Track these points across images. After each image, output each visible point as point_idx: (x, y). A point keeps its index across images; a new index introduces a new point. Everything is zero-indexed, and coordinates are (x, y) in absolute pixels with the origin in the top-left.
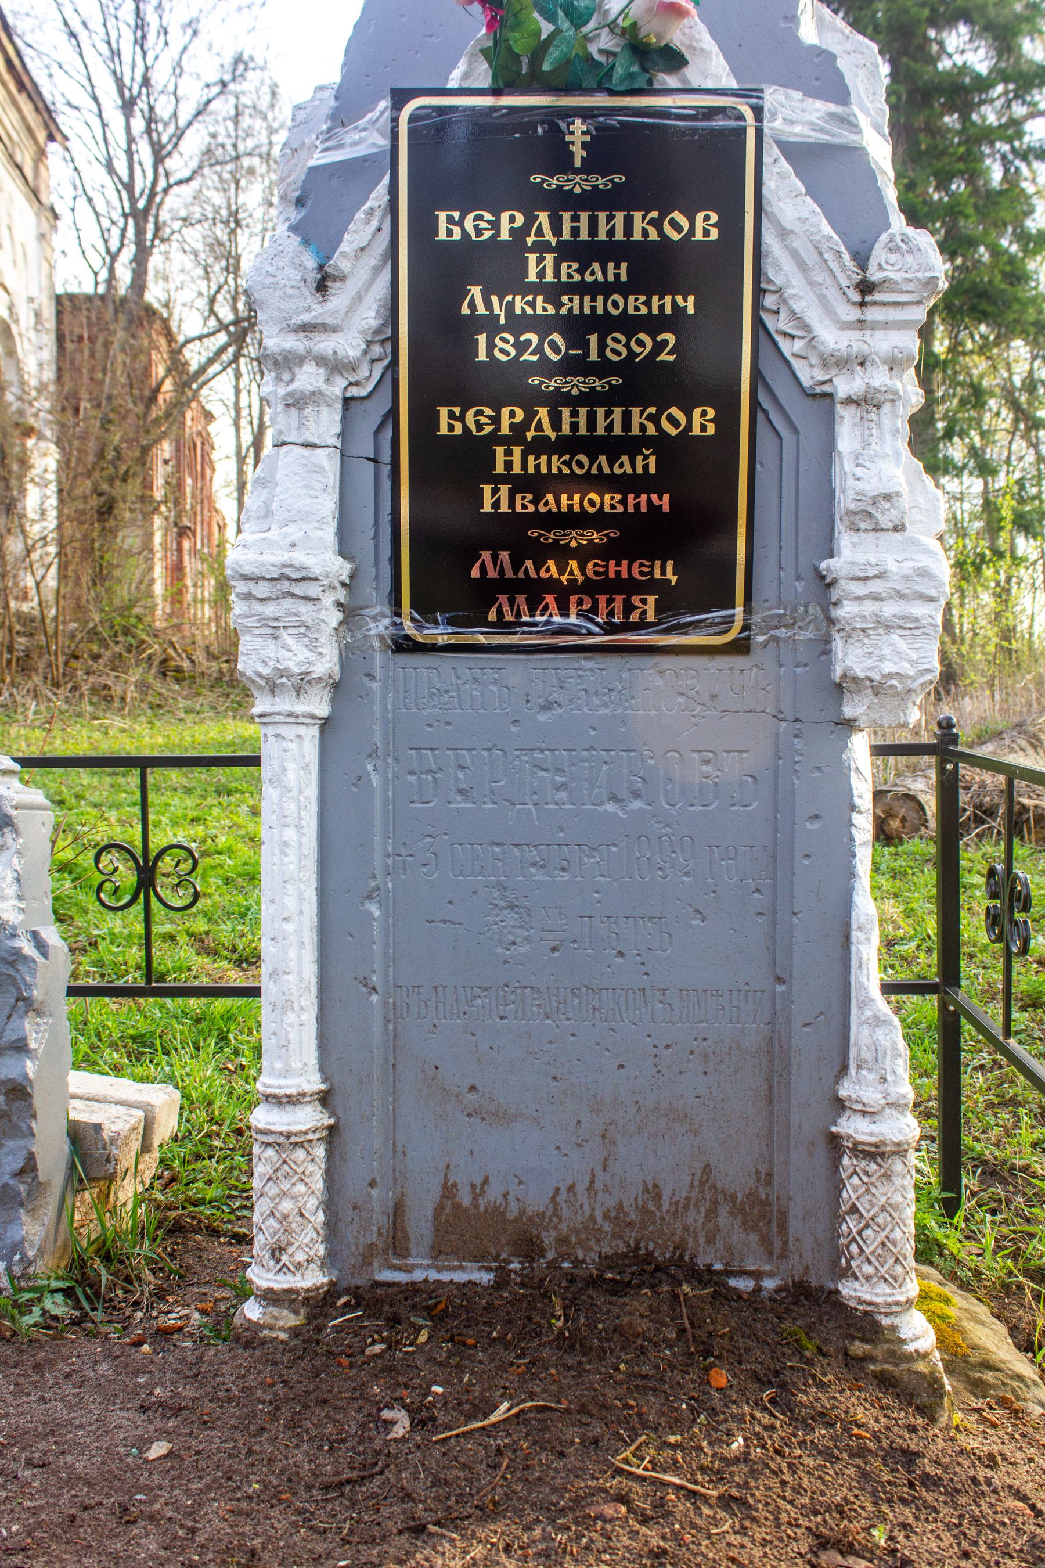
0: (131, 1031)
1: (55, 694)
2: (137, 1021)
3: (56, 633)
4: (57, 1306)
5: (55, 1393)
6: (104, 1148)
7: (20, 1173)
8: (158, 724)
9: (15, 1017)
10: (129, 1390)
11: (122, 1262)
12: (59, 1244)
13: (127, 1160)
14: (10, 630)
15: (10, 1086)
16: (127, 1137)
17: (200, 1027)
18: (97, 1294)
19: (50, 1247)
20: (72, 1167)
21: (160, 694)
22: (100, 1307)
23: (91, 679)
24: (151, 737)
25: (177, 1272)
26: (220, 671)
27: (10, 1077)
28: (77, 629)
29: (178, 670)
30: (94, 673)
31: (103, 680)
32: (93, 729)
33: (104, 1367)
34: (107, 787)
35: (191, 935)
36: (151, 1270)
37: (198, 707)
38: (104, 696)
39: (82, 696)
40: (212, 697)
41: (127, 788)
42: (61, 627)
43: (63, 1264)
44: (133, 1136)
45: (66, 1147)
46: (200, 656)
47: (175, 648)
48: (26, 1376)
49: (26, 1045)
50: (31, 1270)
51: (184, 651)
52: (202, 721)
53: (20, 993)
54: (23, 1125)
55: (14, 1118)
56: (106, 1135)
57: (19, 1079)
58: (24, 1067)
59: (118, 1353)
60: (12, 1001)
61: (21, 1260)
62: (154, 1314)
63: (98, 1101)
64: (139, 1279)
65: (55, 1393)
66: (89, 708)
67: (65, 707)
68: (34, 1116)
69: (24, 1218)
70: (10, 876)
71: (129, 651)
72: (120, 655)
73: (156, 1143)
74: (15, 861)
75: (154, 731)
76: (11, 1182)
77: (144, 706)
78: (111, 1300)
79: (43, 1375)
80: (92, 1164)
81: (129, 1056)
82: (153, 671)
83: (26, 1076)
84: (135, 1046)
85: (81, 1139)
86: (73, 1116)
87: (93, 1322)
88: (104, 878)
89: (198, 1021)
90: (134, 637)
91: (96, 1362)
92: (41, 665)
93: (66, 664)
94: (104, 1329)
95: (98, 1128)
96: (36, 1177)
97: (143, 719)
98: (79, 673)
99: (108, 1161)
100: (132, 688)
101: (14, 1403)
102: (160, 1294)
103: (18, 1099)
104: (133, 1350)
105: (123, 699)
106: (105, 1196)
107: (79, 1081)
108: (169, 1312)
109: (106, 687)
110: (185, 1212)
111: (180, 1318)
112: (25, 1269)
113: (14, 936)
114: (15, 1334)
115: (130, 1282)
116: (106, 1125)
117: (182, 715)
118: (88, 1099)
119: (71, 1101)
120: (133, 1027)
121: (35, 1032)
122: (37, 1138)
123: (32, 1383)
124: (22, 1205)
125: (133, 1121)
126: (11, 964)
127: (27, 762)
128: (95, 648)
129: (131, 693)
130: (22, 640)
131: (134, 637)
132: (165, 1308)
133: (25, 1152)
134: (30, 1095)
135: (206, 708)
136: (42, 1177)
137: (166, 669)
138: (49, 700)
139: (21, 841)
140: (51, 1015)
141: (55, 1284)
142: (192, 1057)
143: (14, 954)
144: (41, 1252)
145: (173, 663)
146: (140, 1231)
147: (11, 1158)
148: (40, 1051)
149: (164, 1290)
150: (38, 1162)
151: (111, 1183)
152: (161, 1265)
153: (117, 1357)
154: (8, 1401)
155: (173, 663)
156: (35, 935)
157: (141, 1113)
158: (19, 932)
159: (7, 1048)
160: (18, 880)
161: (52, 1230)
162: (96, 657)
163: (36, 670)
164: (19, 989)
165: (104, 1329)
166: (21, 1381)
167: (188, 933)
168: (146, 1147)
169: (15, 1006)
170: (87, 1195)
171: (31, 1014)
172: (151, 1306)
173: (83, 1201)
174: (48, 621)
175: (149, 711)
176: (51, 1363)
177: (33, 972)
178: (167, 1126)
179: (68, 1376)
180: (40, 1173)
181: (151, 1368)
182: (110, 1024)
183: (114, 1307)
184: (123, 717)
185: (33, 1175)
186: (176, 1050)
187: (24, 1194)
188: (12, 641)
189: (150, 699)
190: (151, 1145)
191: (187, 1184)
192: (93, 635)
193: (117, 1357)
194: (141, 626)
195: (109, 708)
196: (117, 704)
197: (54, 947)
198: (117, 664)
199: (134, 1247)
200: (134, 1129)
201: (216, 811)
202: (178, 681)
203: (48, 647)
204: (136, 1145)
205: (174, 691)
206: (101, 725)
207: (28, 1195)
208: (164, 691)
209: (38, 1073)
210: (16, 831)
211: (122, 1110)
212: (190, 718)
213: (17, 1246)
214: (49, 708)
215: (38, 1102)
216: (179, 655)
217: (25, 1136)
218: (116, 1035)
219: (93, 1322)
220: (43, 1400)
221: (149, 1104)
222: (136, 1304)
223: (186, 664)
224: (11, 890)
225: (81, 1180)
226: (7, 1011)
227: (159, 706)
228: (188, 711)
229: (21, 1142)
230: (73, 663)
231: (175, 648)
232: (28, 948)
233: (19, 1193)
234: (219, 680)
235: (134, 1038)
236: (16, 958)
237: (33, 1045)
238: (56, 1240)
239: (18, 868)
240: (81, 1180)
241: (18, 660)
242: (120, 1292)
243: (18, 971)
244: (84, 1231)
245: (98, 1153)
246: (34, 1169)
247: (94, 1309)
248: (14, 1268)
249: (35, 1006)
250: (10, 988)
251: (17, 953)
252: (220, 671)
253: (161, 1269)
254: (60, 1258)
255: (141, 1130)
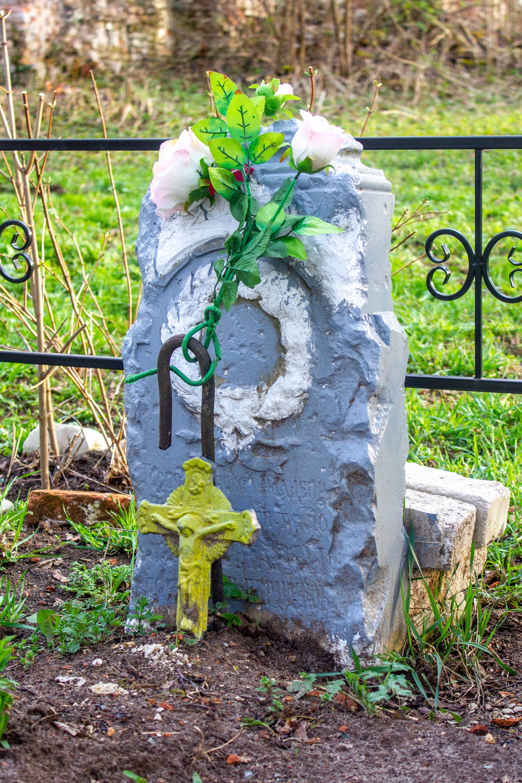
0: (444, 428)
1: (344, 84)
2: (448, 419)
3: (344, 21)
4: (397, 685)
5: (403, 768)
6: (439, 540)
7: (361, 556)
8: (447, 114)
9: (357, 401)
10: (476, 774)
11: (455, 653)
12: (395, 629)
13: (462, 550)
14: (300, 17)
15: (352, 470)
16: (460, 531)
17: (513, 428)
18: (433, 683)
19: (386, 632)
20: (407, 555)
21: (449, 82)
22: (437, 694)
23: (380, 68)
24: (442, 128)
25: (508, 669)
26: (513, 57)
27: (352, 460)
28: (365, 16)
29: (468, 56)
30: (382, 61)
31: (391, 69)
32: (383, 120)
33: (449, 750)
34: (398, 181)
35: (497, 334)
36: (483, 664)
37: (489, 96)
38: (393, 86)
39: (370, 85)
40: (503, 84)
41: (420, 182)
42: (350, 14)
43: (398, 649)
44: (466, 531)
45: (401, 535)
46: (490, 40)
47: (465, 34)
48: (376, 749)
49: (368, 430)
50: (370, 650)
51: (475, 36)
52: (493, 111)
53: (363, 377)
54: (363, 509)
55: (356, 502)
56: (441, 526)
57: (361, 463)
58: (366, 452)
59: (463, 738)
60: (355, 385)
61: (361, 640)
62: (488, 707)
63: (429, 492)
64: (472, 673)
65: (403, 768)
66: (378, 99)
67: (352, 97)
68: (374, 501)
69: (364, 600)
70: (355, 258)
71: (419, 37)
72: (409, 42)
73: (487, 539)
74: (360, 243)
75: (445, 122)
76: (352, 564)
77: (434, 95)
78: (445, 688)
79: (391, 750)
80: (426, 554)
81: (443, 451)
82: (443, 58)
83: (368, 461)
84: (448, 443)
85: (415, 526)
86: (407, 506)
87: (430, 707)
88: (436, 265)
89: (511, 422)
90: (424, 21)
91: (441, 745)
92: (330, 53)
93: (355, 52)
94: (442, 715)
95: (433, 518)
96: (375, 561)
97: (432, 109)
98: (368, 61)
99: (442, 552)
100: (421, 76)
101: (366, 772)
102: (492, 688)
103: (360, 483)
104: (477, 738)
105: (412, 89)
106: (434, 588)
107: (415, 473)
108: (503, 707)
109: (394, 76)
110: (512, 611)
111: (515, 714)
112: (364, 649)
113: (357, 320)
114: (360, 708)
115: (463, 674)
116: (441, 517)
117: (472, 104)
118: (420, 490)
119: (407, 490)
120: (446, 424)
121: (375, 417)
122: (377, 523)
123: (382, 756)
124: (362, 587)
125: (466, 515)
126: (355, 347)
127: (370, 144)
128: (383, 35)
129: (421, 81)
130: (311, 28)
131: (424, 21)
132: (498, 702)
133: (365, 536)
134: (371, 480)
135: (498, 97)
136: (381, 562)
137: (456, 56)
138: (338, 91)
139: (365, 222)
140: (391, 402)
141: (397, 667)
142: (506, 459)
143: (357, 338)
144: (379, 634)
145: (463, 50)
146: (469, 624)
147: (351, 540)
148: (381, 437)
149: (496, 685)
150: (378, 547)
151: (442, 574)
152: (492, 660)
153: (462, 742)
154: (361, 770)
155: (463, 50)
156: (377, 319)
157: (473, 508)
158: (362, 315)
159: (349, 432)
160: (362, 262)
161: (389, 614)
162: (385, 44)
163: (324, 60)
164: (361, 373)
165: (442, 715)
166: (371, 752)
167: (494, 333)
168: (477, 544)
169: (358, 390)
170: (420, 584)
171: (372, 399)
172: (484, 700)
173: (416, 590)
174: (337, 8)
175: (438, 102)
176: (399, 740)
177: (376, 357)
178: (496, 525)
179: (415, 754)
180: (378, 558)
181: (497, 756)
182: (422, 420)
183: (449, 696)
184: (412, 107)
185: (372, 559)
186: (490, 450)
187: (364, 577)
188: (301, 29)
189: (439, 88)
190: (482, 541)
191: (513, 584)
192: (383, 22)
193: (462, 742)
194: (431, 10)
195: (398, 98)
196: (406, 94)
197: (395, 333)
198: (406, 50)
199: (467, 640)
200: (467, 523)
201: (513, 206)
202: (468, 68)
203: (337, 35)
204: (468, 540)
205: (463, 80)
206: (390, 116)
207: (368, 578)
208: (453, 79)
209: (379, 458)
210: (361, 212)
211: (455, 503)
212: (481, 108)
213: (357, 627)
214: (338, 99)
215: (378, 487)
216: (469, 41)
217: (365, 521)
218: (428, 432)
219: (430, 707)
220: (392, 772)
221: (481, 500)
222: (470, 695)
223: (476, 51)
224: (356, 273)
225: (415, 569)
226: (350, 395)
227: (449, 96)
228: (480, 100)
229: (362, 526)
230: (362, 52)
231: (465, 34)
232: (371, 334)
233: (359, 575)
234: (511, 66)
235: (447, 436)
236: (359, 342)
237: (374, 430)
238: (392, 625)
239: (362, 250)
240: (415, 569)
241: (307, 48)
242: (454, 682)
243: (361, 355)
244: (417, 619)
245: (432, 544)
246: (374, 553)
247: (430, 695)
248: (355, 647)
249: (377, 391)
250: (353, 372)
251: (361, 336)
252: (513, 57)
253: (492, 664)
254: (396, 643)
255: (473, 525)
